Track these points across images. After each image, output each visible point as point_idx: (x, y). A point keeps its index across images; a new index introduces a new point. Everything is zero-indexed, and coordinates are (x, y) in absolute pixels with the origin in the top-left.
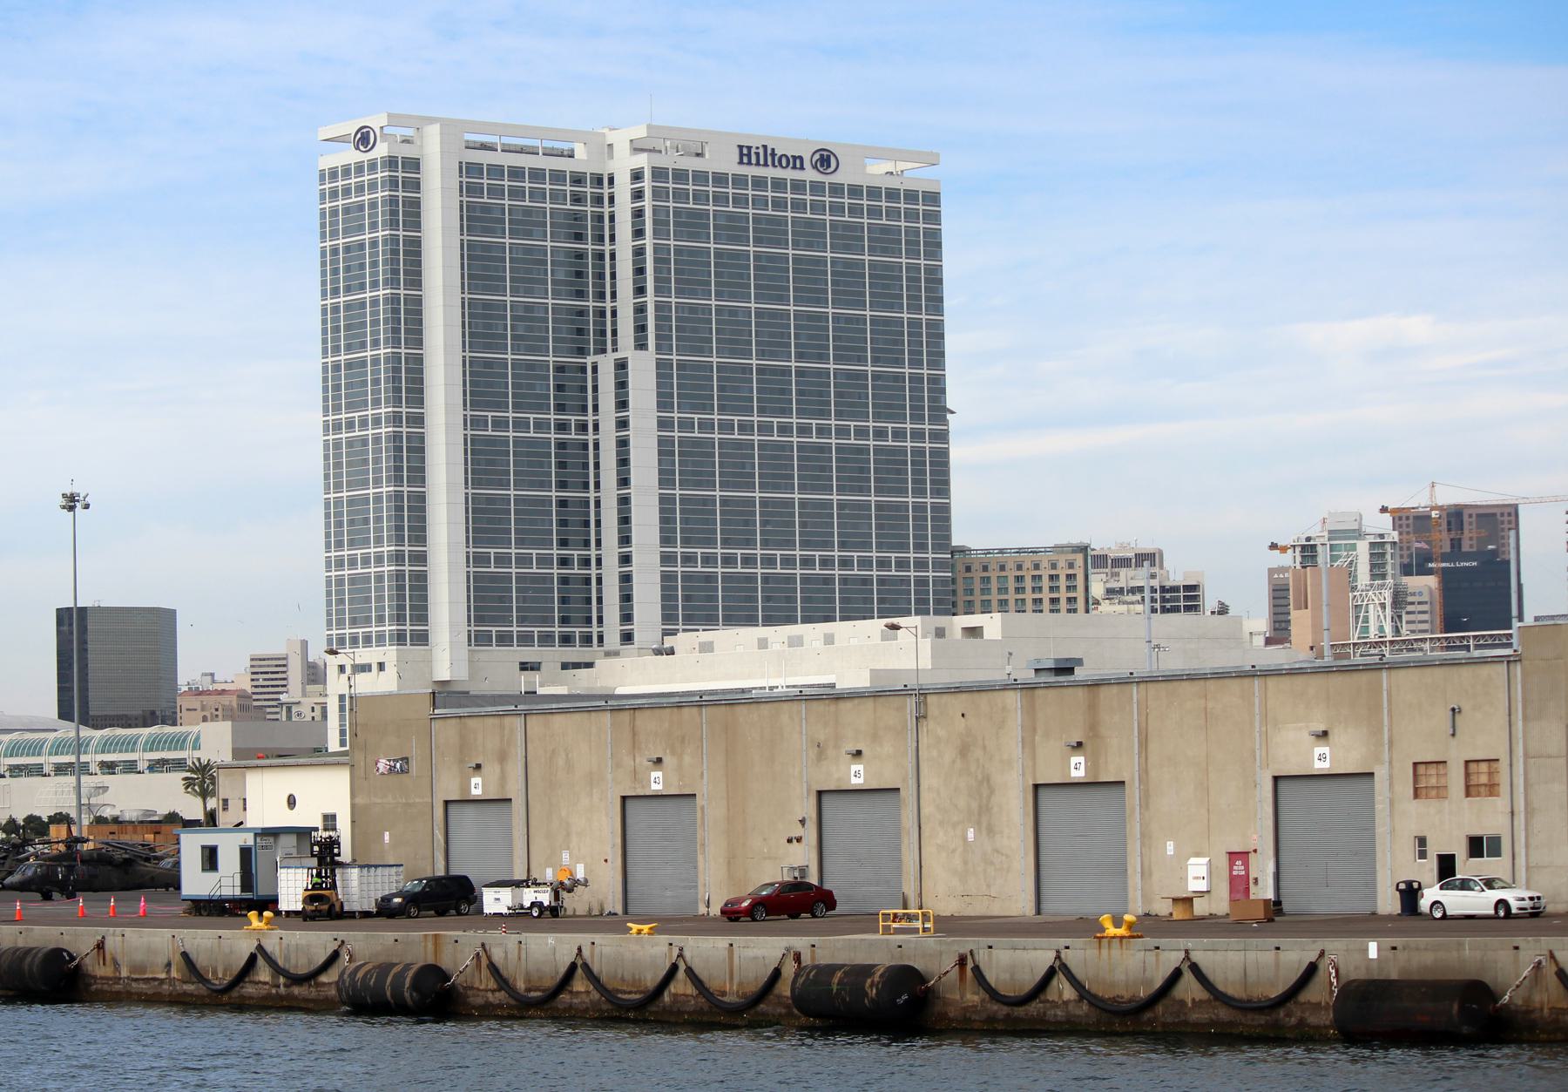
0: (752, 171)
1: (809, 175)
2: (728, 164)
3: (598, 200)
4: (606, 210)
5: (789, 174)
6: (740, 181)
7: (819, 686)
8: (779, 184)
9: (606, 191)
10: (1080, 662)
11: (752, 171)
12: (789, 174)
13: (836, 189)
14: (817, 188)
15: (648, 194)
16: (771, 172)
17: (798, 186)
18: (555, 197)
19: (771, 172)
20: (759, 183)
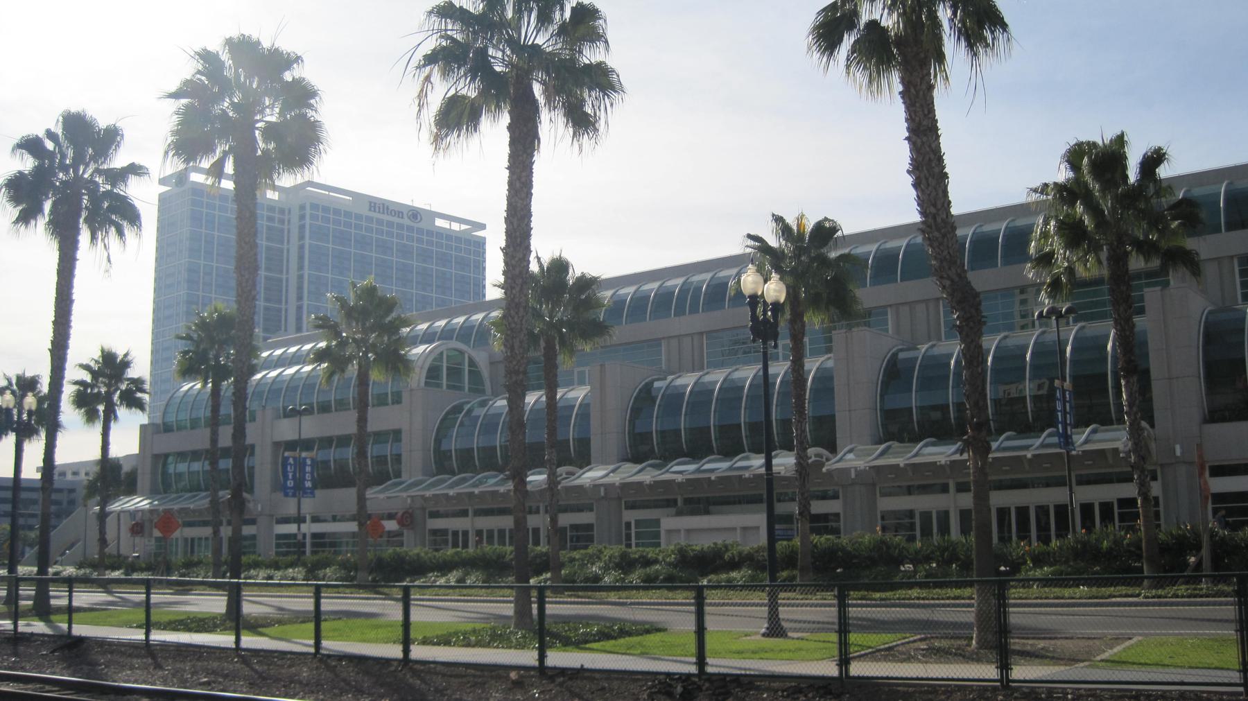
0: (375, 215)
1: (406, 222)
2: (365, 211)
3: (282, 221)
4: (286, 227)
5: (396, 220)
6: (369, 219)
7: (740, 669)
8: (390, 224)
9: (286, 218)
10: (298, 59)
11: (375, 215)
12: (396, 220)
13: (420, 231)
14: (410, 229)
15: (308, 217)
16: (386, 217)
17: (401, 227)
18: (357, 227)
19: (386, 217)
20: (380, 222)
